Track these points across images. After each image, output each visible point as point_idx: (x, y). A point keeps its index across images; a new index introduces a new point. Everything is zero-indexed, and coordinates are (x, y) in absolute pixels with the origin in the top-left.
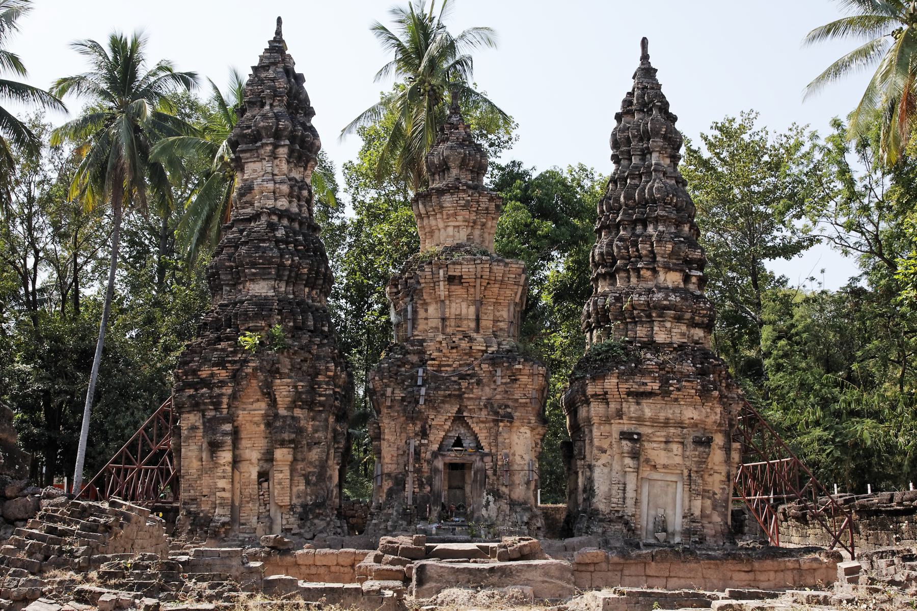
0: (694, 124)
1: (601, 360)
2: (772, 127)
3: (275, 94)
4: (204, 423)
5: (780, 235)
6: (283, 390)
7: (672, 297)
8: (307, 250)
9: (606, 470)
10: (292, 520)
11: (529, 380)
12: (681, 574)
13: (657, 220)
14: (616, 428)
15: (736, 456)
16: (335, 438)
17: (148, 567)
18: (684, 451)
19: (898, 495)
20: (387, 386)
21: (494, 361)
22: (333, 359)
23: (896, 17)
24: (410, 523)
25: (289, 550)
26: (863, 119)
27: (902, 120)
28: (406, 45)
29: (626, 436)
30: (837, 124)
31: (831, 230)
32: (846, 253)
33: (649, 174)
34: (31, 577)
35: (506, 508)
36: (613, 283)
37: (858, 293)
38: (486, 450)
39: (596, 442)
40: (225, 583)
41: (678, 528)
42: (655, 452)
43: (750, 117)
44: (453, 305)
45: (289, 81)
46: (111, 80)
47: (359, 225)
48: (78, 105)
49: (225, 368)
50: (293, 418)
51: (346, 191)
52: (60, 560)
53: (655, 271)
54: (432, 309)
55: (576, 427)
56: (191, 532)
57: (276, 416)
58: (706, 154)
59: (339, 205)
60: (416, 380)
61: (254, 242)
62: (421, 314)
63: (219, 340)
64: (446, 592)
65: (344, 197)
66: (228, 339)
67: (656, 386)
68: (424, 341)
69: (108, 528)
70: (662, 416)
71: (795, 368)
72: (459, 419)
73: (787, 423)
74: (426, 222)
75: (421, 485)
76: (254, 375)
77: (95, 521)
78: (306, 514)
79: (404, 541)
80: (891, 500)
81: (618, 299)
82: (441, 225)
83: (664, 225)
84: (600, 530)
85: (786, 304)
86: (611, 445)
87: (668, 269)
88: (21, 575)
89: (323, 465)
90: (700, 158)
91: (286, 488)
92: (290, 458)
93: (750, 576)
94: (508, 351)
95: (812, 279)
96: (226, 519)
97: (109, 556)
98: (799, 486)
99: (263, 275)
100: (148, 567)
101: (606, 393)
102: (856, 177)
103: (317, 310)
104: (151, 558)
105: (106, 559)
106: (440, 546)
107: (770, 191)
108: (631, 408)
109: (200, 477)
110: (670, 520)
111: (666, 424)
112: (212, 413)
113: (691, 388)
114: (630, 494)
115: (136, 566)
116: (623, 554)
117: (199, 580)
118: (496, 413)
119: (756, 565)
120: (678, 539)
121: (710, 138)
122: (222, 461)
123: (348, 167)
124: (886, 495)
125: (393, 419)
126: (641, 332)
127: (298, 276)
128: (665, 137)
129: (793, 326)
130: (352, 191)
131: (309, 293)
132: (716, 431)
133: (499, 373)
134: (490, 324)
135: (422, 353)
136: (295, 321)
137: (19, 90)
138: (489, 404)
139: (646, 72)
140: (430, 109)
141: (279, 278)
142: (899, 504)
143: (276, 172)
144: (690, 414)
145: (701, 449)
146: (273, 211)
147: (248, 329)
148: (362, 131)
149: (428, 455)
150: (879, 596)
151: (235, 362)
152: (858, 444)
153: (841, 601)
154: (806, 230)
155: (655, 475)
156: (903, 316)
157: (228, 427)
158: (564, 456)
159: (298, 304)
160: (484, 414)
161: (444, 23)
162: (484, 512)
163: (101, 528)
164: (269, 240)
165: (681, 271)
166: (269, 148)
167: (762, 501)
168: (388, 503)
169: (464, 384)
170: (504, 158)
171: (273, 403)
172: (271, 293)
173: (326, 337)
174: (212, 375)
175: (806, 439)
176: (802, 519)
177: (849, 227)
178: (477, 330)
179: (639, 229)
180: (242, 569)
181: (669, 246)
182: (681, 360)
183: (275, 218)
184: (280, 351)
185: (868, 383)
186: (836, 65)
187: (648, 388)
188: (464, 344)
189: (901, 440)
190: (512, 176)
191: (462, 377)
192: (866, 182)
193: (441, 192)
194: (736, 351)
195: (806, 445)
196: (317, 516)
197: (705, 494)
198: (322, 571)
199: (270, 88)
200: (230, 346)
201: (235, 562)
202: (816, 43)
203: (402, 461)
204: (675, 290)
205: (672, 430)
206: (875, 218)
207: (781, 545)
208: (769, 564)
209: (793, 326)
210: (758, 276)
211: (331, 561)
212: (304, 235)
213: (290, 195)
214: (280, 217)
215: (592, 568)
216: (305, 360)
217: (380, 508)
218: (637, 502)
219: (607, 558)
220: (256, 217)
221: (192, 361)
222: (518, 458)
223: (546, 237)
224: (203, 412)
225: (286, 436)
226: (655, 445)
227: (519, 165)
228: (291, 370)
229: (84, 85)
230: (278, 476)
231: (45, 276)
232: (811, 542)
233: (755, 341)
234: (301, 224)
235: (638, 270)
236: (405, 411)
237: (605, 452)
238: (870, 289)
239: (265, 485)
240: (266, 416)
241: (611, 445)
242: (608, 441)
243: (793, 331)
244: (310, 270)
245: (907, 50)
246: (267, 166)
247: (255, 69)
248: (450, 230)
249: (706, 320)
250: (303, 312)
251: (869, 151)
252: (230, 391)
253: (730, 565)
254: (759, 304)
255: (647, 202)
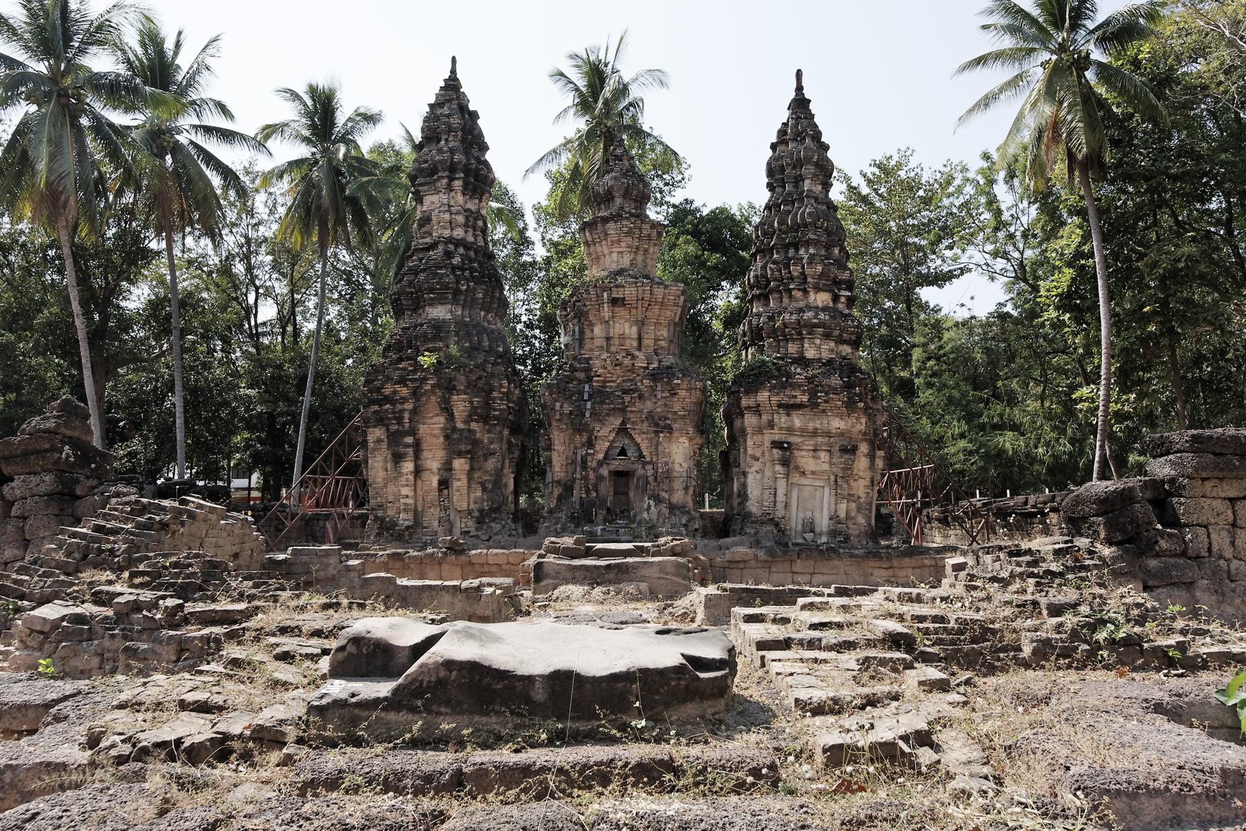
0: (852, 156)
1: (755, 375)
2: (927, 164)
3: (450, 129)
4: (388, 437)
5: (935, 264)
6: (460, 405)
7: (822, 316)
8: (483, 277)
9: (758, 476)
10: (470, 523)
11: (685, 399)
12: (825, 571)
13: (808, 243)
14: (768, 437)
15: (880, 463)
16: (509, 449)
17: (191, 565)
18: (831, 458)
19: (1032, 499)
20: (556, 401)
21: (655, 376)
22: (507, 377)
23: (1047, 48)
24: (577, 526)
25: (464, 550)
26: (1011, 150)
27: (1048, 148)
28: (584, 89)
29: (777, 445)
30: (986, 157)
31: (979, 258)
32: (992, 279)
33: (801, 200)
34: (62, 577)
35: (666, 511)
36: (767, 304)
37: (1003, 317)
38: (648, 459)
39: (750, 451)
40: (271, 582)
41: (825, 529)
42: (806, 460)
43: (906, 155)
44: (617, 325)
45: (463, 118)
46: (313, 127)
47: (548, 261)
48: (288, 150)
49: (406, 385)
50: (470, 431)
51: (535, 230)
52: (99, 559)
53: (805, 292)
54: (598, 330)
55: (732, 437)
56: (378, 535)
57: (454, 429)
58: (865, 190)
59: (527, 243)
60: (584, 393)
61: (432, 269)
62: (588, 334)
63: (401, 360)
64: (562, 588)
65: (533, 234)
66: (409, 359)
67: (805, 398)
68: (590, 359)
69: (164, 526)
70: (811, 426)
71: (945, 385)
72: (623, 431)
73: (934, 437)
74: (592, 248)
75: (588, 491)
76: (432, 391)
77: (150, 518)
78: (482, 518)
79: (568, 541)
80: (1026, 503)
81: (771, 318)
82: (606, 251)
83: (815, 248)
84: (752, 531)
85: (937, 327)
86: (763, 453)
87: (818, 289)
88: (51, 575)
89: (499, 474)
90: (860, 193)
91: (464, 495)
92: (467, 467)
93: (890, 572)
94: (668, 367)
95: (963, 305)
96: (410, 523)
97: (151, 554)
98: (944, 493)
99: (441, 300)
100: (191, 565)
101: (759, 405)
102: (1003, 207)
103: (492, 331)
104: (197, 556)
105: (148, 558)
106: (599, 546)
107: (923, 224)
108: (782, 420)
109: (385, 486)
110: (817, 521)
111: (815, 433)
112: (396, 427)
113: (838, 401)
114: (781, 498)
115: (175, 565)
116: (771, 552)
117: (245, 579)
118: (657, 425)
119: (895, 563)
120: (824, 539)
121: (869, 174)
122: (405, 471)
123: (537, 208)
124: (1021, 498)
125: (562, 431)
126: (792, 348)
127: (474, 300)
128: (817, 165)
129: (941, 347)
130: (541, 230)
131: (485, 316)
132: (862, 440)
133: (659, 388)
134: (651, 343)
135: (588, 370)
136: (471, 342)
137: (227, 136)
138: (650, 416)
139: (800, 104)
140: (606, 149)
141: (455, 301)
142: (1033, 507)
143: (452, 203)
144: (837, 424)
145: (846, 456)
146: (450, 240)
147: (427, 350)
148: (548, 174)
149: (594, 464)
150: (974, 594)
151: (415, 380)
152: (1001, 452)
153: (934, 599)
154: (955, 259)
155: (804, 481)
156: (1045, 337)
157: (409, 440)
158: (721, 468)
159: (474, 326)
160: (645, 424)
161: (618, 67)
162: (645, 515)
163: (157, 526)
164: (445, 267)
165: (829, 291)
166: (445, 181)
167: (907, 505)
168: (558, 508)
169: (627, 398)
170: (677, 197)
171: (451, 417)
172: (448, 316)
173: (501, 357)
174: (395, 392)
175: (952, 450)
176: (944, 522)
177: (995, 254)
178: (639, 348)
179: (791, 252)
180: (340, 567)
181: (819, 268)
182: (827, 375)
183: (451, 247)
184: (457, 370)
185: (1012, 400)
186: (986, 97)
187: (798, 401)
188: (627, 361)
189: (1040, 450)
190: (683, 214)
191: (625, 392)
192: (1013, 212)
193: (605, 220)
194: (891, 371)
195: (954, 455)
196: (493, 520)
197: (850, 497)
198: (494, 569)
199: (445, 123)
200: (410, 365)
201: (333, 560)
202: (966, 73)
203: (570, 469)
204: (825, 309)
205: (820, 439)
206: (1021, 246)
207: (925, 544)
208: (907, 561)
209: (941, 347)
210: (911, 302)
211: (503, 560)
212: (479, 263)
213: (466, 225)
214: (457, 246)
215: (741, 566)
216: (480, 378)
217: (551, 512)
218: (787, 505)
219: (756, 556)
220: (433, 246)
221: (376, 379)
222: (677, 467)
223: (715, 267)
224: (387, 426)
225: (463, 447)
226: (804, 453)
227: (692, 202)
228: (467, 387)
229: (288, 131)
230: (456, 484)
231: (267, 312)
232: (952, 541)
233: (907, 364)
234: (476, 252)
235: (790, 291)
236: (572, 424)
237: (757, 459)
238: (1015, 313)
239: (445, 492)
240: (444, 429)
241: (763, 453)
242: (760, 450)
243: (941, 352)
244: (485, 295)
245: (1055, 79)
246: (443, 198)
247: (431, 106)
248: (615, 255)
249: (854, 337)
250: (479, 334)
251: (1016, 182)
252: (411, 407)
253: (872, 563)
254: (912, 329)
255: (799, 227)
